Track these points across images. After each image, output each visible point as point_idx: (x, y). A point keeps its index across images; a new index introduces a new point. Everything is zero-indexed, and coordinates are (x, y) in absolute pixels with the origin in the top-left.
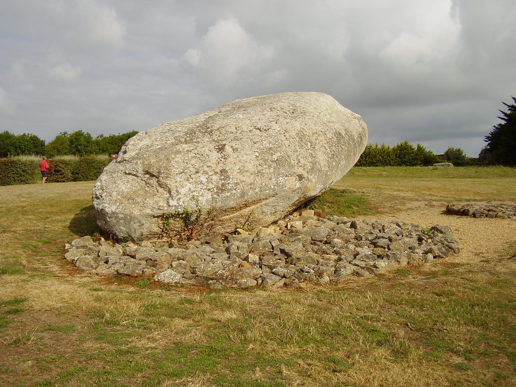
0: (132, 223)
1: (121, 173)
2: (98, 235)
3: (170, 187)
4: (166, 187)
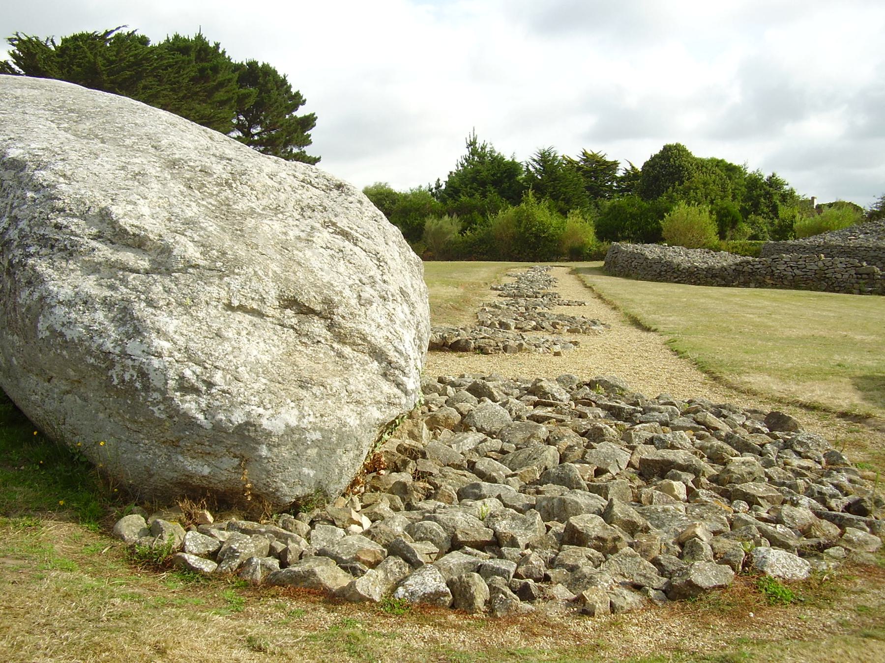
0: (339, 451)
1: (216, 307)
2: (186, 504)
3: (373, 341)
4: (360, 342)
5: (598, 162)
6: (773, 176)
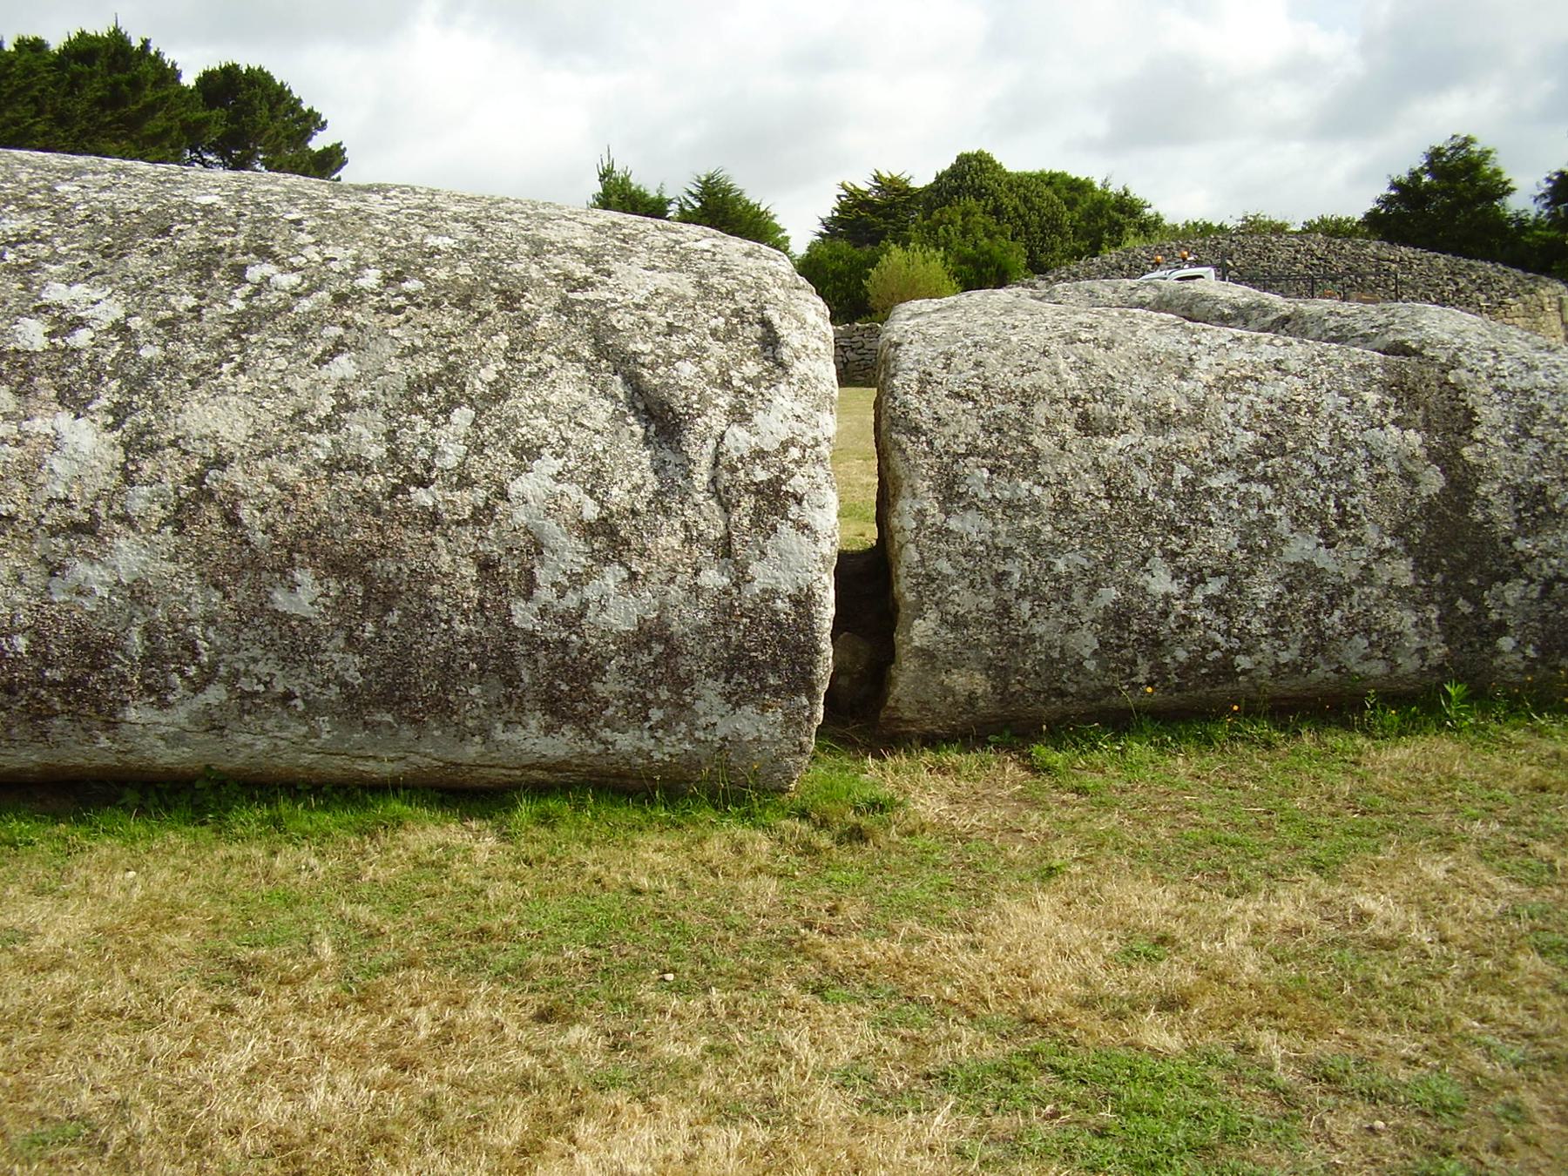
5: (897, 190)
6: (1126, 194)
